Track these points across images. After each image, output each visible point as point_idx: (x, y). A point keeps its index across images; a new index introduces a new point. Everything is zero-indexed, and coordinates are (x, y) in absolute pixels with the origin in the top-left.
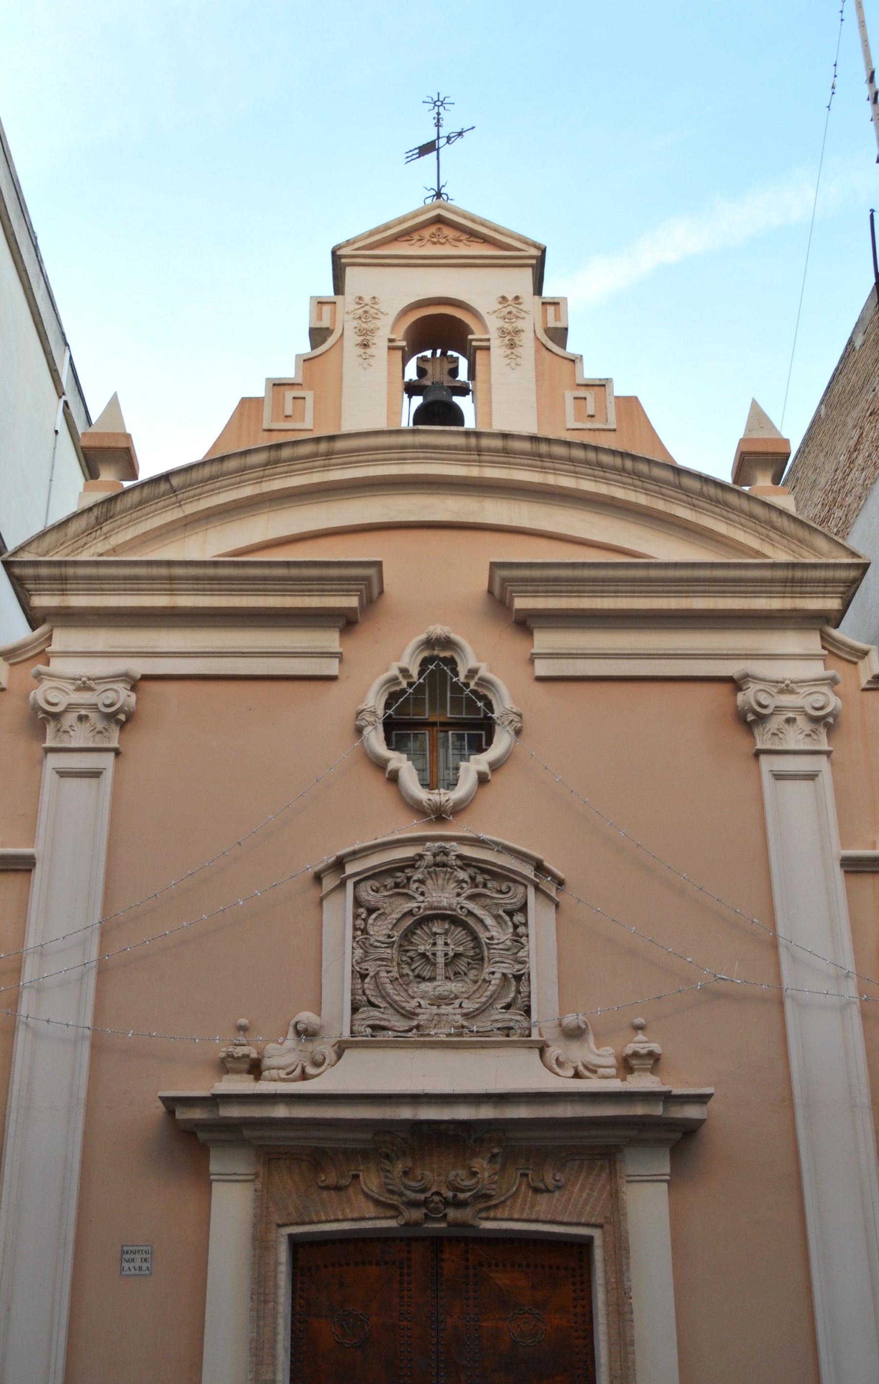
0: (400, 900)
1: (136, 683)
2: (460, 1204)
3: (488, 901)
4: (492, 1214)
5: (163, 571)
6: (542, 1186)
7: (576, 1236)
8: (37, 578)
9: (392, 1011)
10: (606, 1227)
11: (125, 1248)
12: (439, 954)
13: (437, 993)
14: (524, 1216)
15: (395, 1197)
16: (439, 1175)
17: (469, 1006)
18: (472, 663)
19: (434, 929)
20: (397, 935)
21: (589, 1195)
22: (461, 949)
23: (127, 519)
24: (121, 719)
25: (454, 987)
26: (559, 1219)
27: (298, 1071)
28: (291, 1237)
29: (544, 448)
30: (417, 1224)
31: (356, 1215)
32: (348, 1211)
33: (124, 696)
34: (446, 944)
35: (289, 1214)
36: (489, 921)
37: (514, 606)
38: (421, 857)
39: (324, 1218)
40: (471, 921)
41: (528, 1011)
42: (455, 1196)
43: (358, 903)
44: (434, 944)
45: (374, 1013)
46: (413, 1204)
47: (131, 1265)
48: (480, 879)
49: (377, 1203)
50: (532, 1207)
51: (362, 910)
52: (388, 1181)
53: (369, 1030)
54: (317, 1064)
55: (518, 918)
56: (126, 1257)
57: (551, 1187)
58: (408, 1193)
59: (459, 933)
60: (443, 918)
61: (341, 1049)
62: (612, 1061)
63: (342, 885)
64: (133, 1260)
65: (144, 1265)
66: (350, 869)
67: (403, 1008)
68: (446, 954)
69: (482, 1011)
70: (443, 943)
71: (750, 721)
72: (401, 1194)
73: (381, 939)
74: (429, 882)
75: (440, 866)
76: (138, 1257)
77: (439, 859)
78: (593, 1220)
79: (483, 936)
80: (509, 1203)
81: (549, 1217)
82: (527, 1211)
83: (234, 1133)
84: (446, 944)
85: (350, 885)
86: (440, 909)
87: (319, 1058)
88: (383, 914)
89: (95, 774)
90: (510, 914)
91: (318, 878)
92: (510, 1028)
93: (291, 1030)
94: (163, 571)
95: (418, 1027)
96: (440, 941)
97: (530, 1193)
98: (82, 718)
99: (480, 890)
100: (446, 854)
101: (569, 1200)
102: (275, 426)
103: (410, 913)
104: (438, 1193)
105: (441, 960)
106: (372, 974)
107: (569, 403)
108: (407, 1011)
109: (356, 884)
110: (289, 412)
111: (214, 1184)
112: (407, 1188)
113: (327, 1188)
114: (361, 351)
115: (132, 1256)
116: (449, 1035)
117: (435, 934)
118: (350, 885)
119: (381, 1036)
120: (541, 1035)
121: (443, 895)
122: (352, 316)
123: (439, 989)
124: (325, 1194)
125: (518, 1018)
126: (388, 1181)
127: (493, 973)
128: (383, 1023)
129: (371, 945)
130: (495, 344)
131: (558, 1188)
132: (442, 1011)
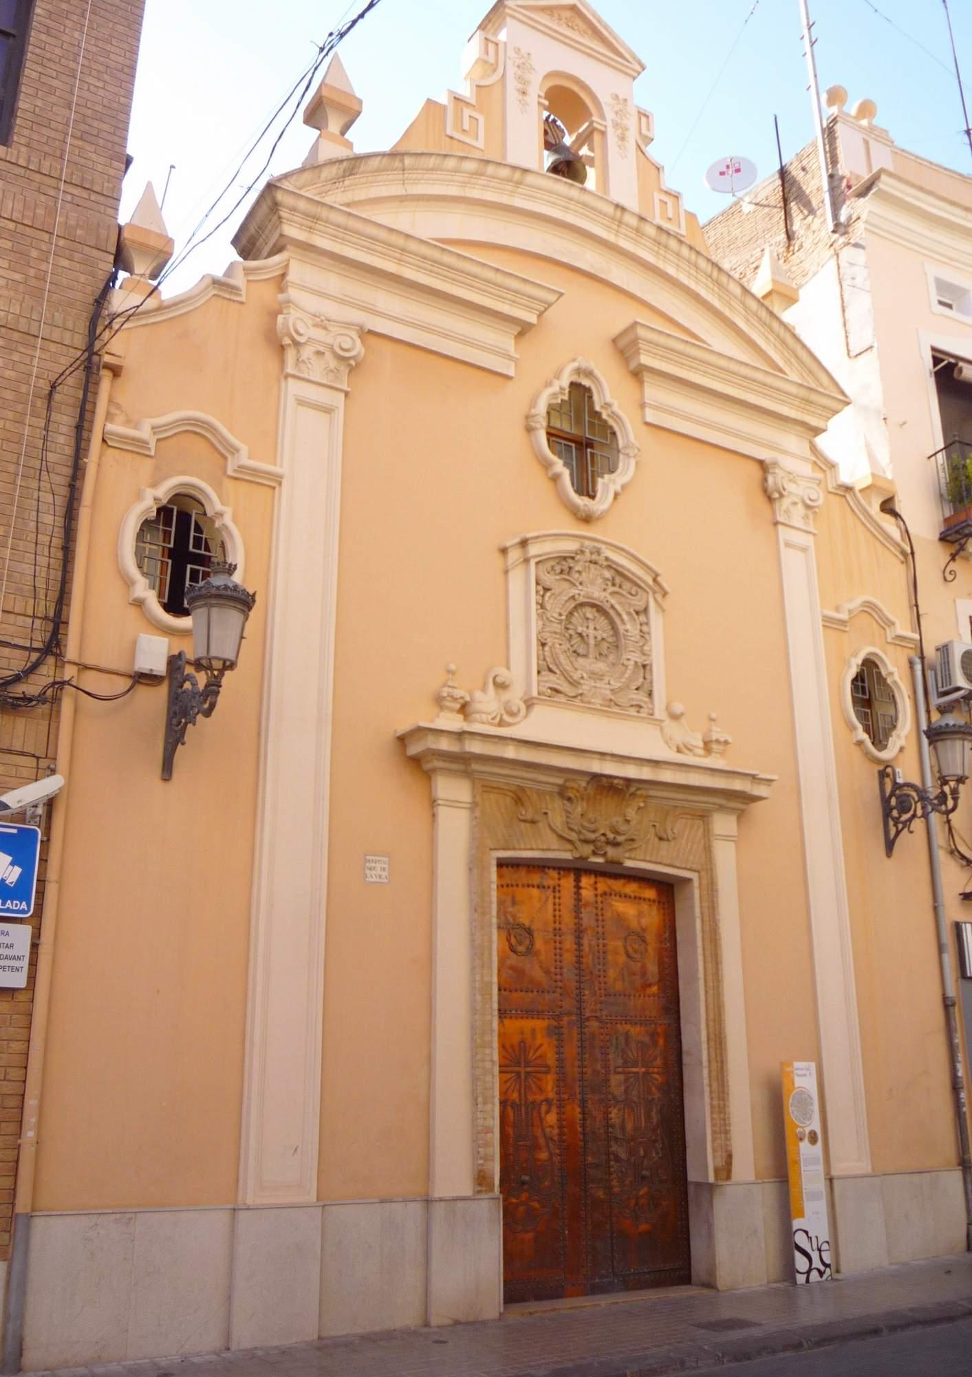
1: (368, 334)
2: (616, 844)
3: (623, 600)
5: (400, 241)
7: (644, 870)
8: (293, 210)
12: (591, 636)
14: (653, 859)
16: (606, 817)
22: (605, 635)
23: (364, 180)
24: (352, 366)
25: (601, 666)
27: (498, 719)
28: (498, 859)
29: (664, 238)
33: (359, 349)
36: (625, 617)
40: (612, 613)
41: (650, 694)
45: (552, 677)
46: (586, 841)
47: (373, 873)
49: (561, 837)
55: (642, 618)
59: (603, 622)
60: (593, 605)
61: (529, 704)
65: (384, 874)
66: (533, 550)
70: (596, 629)
72: (579, 833)
76: (378, 866)
78: (695, 867)
79: (621, 628)
83: (462, 763)
87: (515, 709)
90: (637, 613)
92: (640, 707)
94: (400, 241)
96: (592, 626)
98: (319, 353)
103: (573, 597)
104: (604, 835)
105: (592, 641)
107: (657, 202)
112: (583, 827)
113: (524, 821)
114: (520, 97)
118: (533, 562)
124: (523, 825)
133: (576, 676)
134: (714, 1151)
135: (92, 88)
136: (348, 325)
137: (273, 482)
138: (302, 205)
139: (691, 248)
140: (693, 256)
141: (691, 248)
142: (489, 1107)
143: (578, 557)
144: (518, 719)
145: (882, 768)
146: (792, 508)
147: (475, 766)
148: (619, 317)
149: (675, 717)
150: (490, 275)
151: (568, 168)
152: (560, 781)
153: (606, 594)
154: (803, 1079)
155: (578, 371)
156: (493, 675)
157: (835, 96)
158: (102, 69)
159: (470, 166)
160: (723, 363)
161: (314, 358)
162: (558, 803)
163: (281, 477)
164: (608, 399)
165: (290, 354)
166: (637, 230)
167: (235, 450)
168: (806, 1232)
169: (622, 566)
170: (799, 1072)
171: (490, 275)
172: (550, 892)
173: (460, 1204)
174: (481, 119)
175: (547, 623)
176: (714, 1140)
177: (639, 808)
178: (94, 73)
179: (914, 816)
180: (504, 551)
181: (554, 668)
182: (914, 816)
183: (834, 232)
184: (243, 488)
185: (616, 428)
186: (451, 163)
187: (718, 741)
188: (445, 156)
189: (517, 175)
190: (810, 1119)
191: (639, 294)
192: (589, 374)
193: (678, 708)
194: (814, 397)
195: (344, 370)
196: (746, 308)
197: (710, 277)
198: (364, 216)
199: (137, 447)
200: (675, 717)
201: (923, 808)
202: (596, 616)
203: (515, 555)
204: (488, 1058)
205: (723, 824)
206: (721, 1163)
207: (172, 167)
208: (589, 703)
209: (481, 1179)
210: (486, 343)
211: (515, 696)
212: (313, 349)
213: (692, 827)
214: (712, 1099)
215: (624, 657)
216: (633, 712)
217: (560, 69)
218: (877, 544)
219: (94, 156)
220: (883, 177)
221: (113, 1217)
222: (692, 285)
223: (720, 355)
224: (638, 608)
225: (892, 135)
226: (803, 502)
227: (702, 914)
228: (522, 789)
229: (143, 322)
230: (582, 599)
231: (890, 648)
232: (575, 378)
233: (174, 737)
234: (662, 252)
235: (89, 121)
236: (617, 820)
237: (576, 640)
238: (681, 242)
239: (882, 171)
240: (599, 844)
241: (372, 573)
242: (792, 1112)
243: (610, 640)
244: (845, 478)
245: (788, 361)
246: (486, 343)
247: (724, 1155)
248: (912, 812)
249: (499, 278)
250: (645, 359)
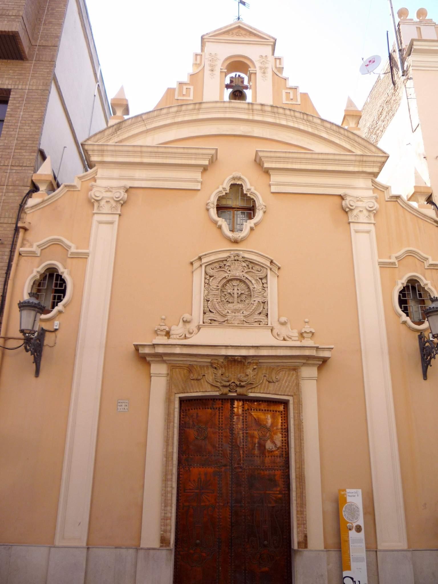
2: (242, 387)
5: (139, 149)
6: (271, 381)
8: (93, 150)
9: (217, 314)
10: (294, 396)
12: (235, 293)
15: (218, 383)
16: (234, 375)
19: (234, 284)
20: (220, 286)
21: (288, 385)
22: (243, 292)
25: (241, 306)
26: (277, 393)
27: (183, 336)
28: (180, 398)
29: (275, 110)
30: (226, 394)
34: (238, 290)
36: (253, 282)
40: (247, 281)
41: (267, 315)
42: (240, 384)
43: (206, 273)
45: (211, 314)
47: (121, 407)
50: (268, 388)
51: (207, 276)
52: (216, 378)
53: (210, 321)
55: (264, 281)
56: (119, 404)
59: (242, 286)
60: (237, 279)
61: (199, 328)
65: (126, 408)
66: (204, 260)
70: (237, 289)
72: (221, 383)
73: (215, 287)
76: (123, 404)
78: (289, 394)
80: (259, 386)
83: (160, 357)
84: (238, 290)
85: (203, 266)
87: (191, 331)
89: (112, 223)
90: (261, 279)
94: (139, 149)
95: (227, 320)
96: (236, 288)
97: (267, 382)
98: (107, 202)
101: (281, 386)
103: (225, 278)
109: (206, 266)
112: (222, 380)
114: (211, 72)
116: (238, 324)
118: (203, 266)
120: (271, 324)
121: (237, 271)
124: (192, 381)
125: (264, 318)
128: (214, 319)
131: (277, 381)
132: (236, 315)
134: (298, 533)
136: (119, 188)
137: (84, 256)
138: (96, 148)
139: (290, 110)
140: (292, 113)
141: (290, 110)
143: (228, 260)
144: (192, 335)
145: (419, 334)
146: (360, 214)
147: (165, 358)
148: (248, 151)
149: (284, 324)
150: (181, 151)
151: (238, 94)
152: (209, 360)
153: (244, 273)
154: (355, 498)
155: (234, 178)
156: (182, 318)
157: (403, 13)
158: (30, 122)
159: (174, 109)
160: (320, 157)
162: (211, 370)
163: (88, 253)
164: (249, 187)
165: (96, 205)
166: (262, 110)
167: (70, 247)
168: (352, 579)
169: (252, 259)
170: (350, 494)
171: (181, 151)
172: (217, 410)
173: (151, 552)
175: (211, 291)
176: (298, 528)
177: (254, 369)
178: (27, 125)
180: (192, 263)
183: (403, 75)
184: (75, 261)
185: (255, 199)
186: (164, 111)
187: (305, 332)
188: (161, 109)
189: (197, 106)
190: (357, 518)
191: (269, 137)
192: (240, 179)
193: (283, 319)
194: (365, 159)
195: (119, 206)
196: (325, 127)
197: (303, 119)
198: (128, 144)
199: (32, 254)
200: (284, 324)
202: (236, 285)
203: (196, 265)
205: (309, 372)
206: (301, 539)
207: (65, 147)
208: (232, 323)
209: (164, 541)
210: (189, 179)
211: (193, 327)
212: (105, 201)
213: (289, 374)
215: (253, 300)
216: (256, 324)
217: (229, 55)
218: (420, 221)
219: (25, 154)
220: (415, 43)
221: (3, 547)
222: (296, 125)
223: (318, 154)
224: (261, 277)
225: (434, 21)
226: (367, 210)
227: (294, 416)
228: (192, 366)
229: (38, 208)
230: (229, 278)
231: (428, 273)
232: (232, 182)
233: (37, 361)
234: (277, 116)
235: (24, 142)
236: (241, 376)
237: (228, 296)
238: (284, 109)
239: (412, 41)
240: (231, 387)
241: (129, 283)
242: (345, 514)
243: (247, 293)
244: (394, 192)
245: (353, 146)
246: (189, 179)
247: (303, 535)
249: (186, 151)
250: (266, 165)
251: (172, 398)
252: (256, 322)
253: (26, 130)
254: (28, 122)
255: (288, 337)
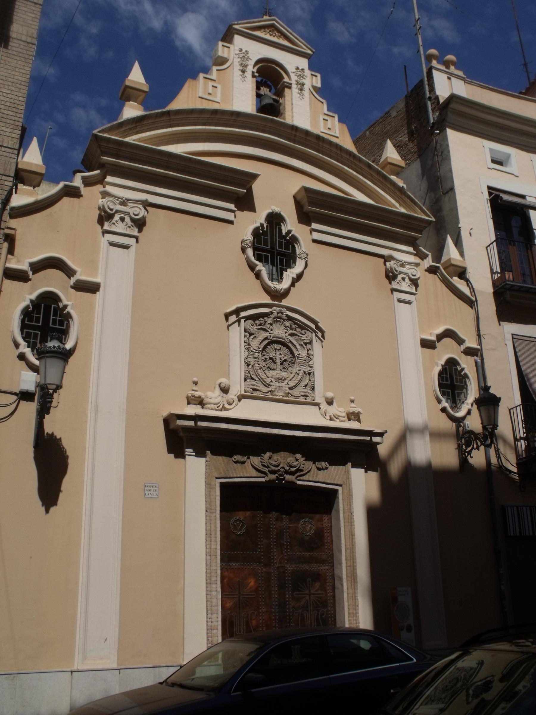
0: (262, 332)
4: (302, 478)
9: (260, 382)
10: (343, 486)
11: (146, 485)
12: (278, 358)
13: (278, 376)
14: (314, 480)
16: (284, 459)
17: (292, 384)
18: (289, 228)
19: (276, 347)
20: (262, 346)
22: (286, 357)
24: (140, 224)
25: (284, 374)
27: (221, 406)
31: (248, 475)
32: (245, 473)
33: (142, 213)
34: (280, 354)
35: (221, 473)
36: (298, 347)
37: (313, 207)
38: (272, 313)
39: (235, 476)
41: (313, 389)
42: (289, 469)
43: (245, 331)
44: (276, 354)
46: (273, 472)
47: (149, 493)
48: (294, 326)
50: (317, 476)
51: (247, 334)
52: (262, 461)
53: (251, 390)
54: (230, 404)
55: (309, 346)
56: (147, 488)
57: (324, 468)
58: (271, 466)
59: (285, 350)
62: (344, 414)
63: (239, 321)
64: (150, 490)
65: (155, 493)
67: (265, 382)
68: (281, 359)
69: (295, 386)
70: (280, 354)
71: (391, 276)
72: (268, 467)
73: (256, 348)
74: (274, 325)
75: (278, 319)
76: (152, 489)
77: (279, 315)
79: (296, 353)
81: (323, 481)
82: (315, 477)
84: (280, 354)
86: (279, 338)
87: (231, 401)
88: (255, 337)
91: (227, 316)
92: (307, 396)
93: (217, 387)
95: (271, 391)
96: (278, 353)
98: (122, 219)
99: (293, 332)
100: (282, 313)
102: (204, 96)
103: (266, 338)
104: (283, 468)
105: (278, 361)
106: (252, 364)
107: (322, 120)
108: (267, 383)
110: (210, 92)
111: (187, 456)
112: (271, 464)
114: (299, 95)
115: (150, 488)
116: (283, 396)
117: (276, 349)
118: (242, 321)
119: (256, 394)
121: (279, 331)
122: (237, 56)
123: (278, 374)
126: (262, 461)
127: (300, 370)
128: (257, 388)
129: (251, 351)
130: (294, 86)
133: (268, 381)
135: (5, 94)
142: (214, 616)
161: (119, 221)
174: (219, 86)
178: (7, 87)
179: (473, 448)
181: (254, 377)
182: (473, 448)
193: (330, 395)
201: (477, 444)
204: (214, 589)
214: (349, 609)
248: (472, 446)
251: (213, 483)
252: (302, 396)
253: (5, 94)
254: (6, 83)
255: (334, 416)
